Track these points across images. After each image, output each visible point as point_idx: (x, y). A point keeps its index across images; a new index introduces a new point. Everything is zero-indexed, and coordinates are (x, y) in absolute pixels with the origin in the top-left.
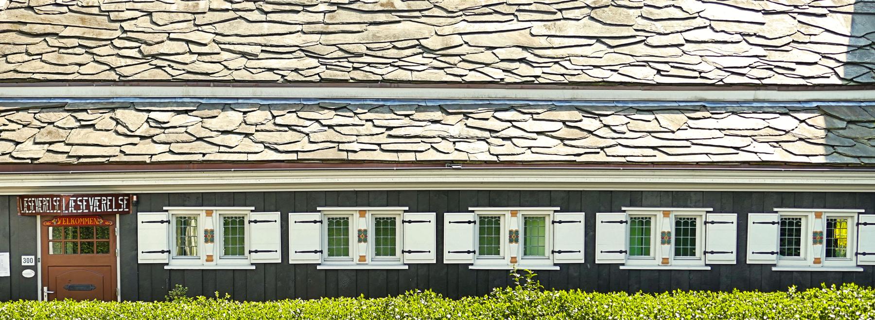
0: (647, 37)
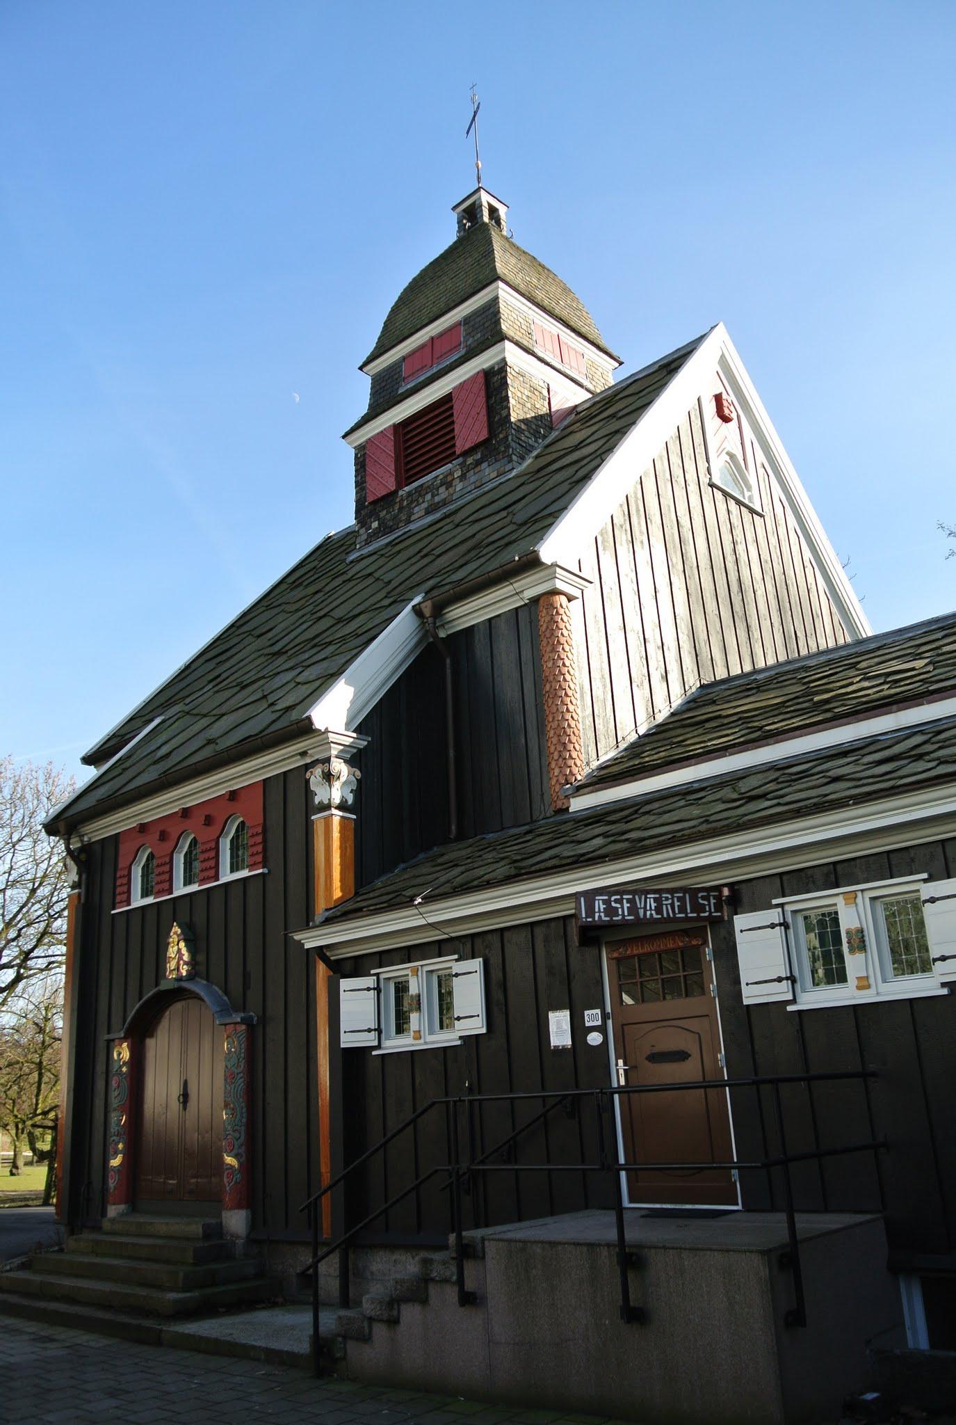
0: (712, 485)
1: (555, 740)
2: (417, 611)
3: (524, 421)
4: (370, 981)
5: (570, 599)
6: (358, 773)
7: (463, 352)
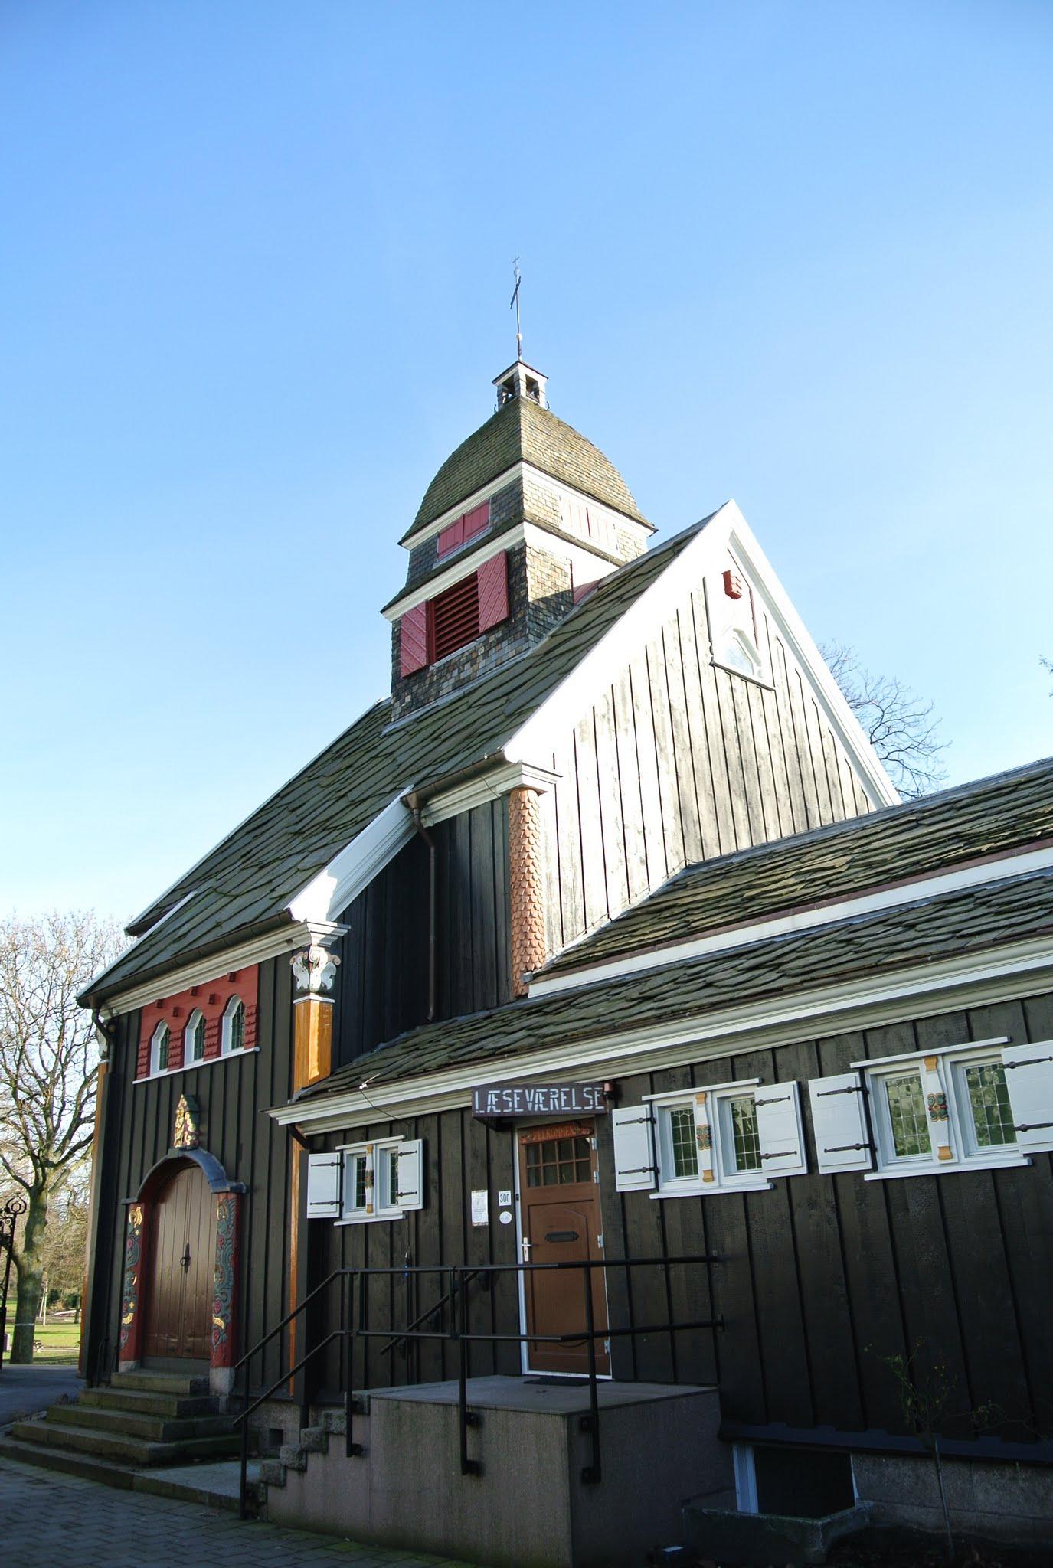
0: (713, 665)
1: (517, 929)
2: (404, 802)
3: (545, 600)
4: (333, 1157)
5: (539, 793)
6: (338, 960)
7: (489, 530)
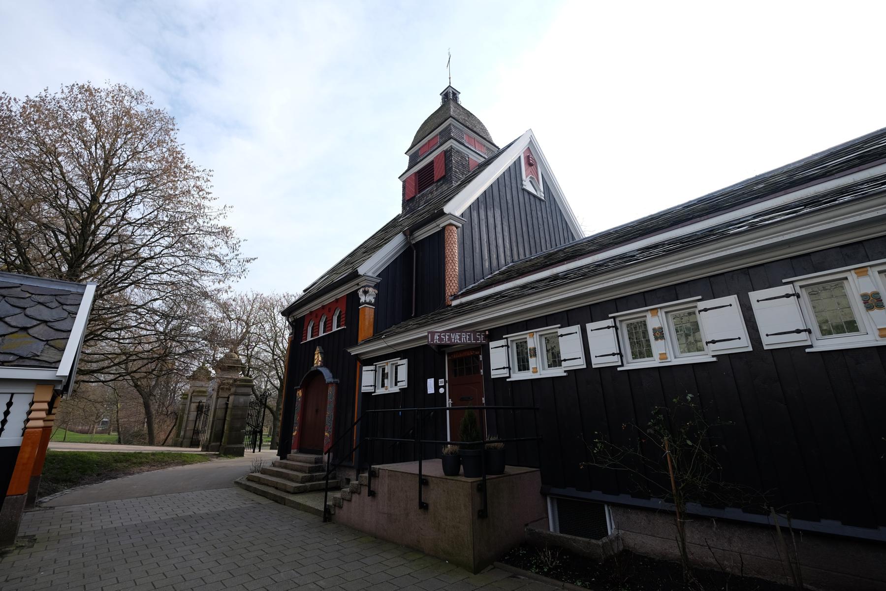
4: (372, 368)
